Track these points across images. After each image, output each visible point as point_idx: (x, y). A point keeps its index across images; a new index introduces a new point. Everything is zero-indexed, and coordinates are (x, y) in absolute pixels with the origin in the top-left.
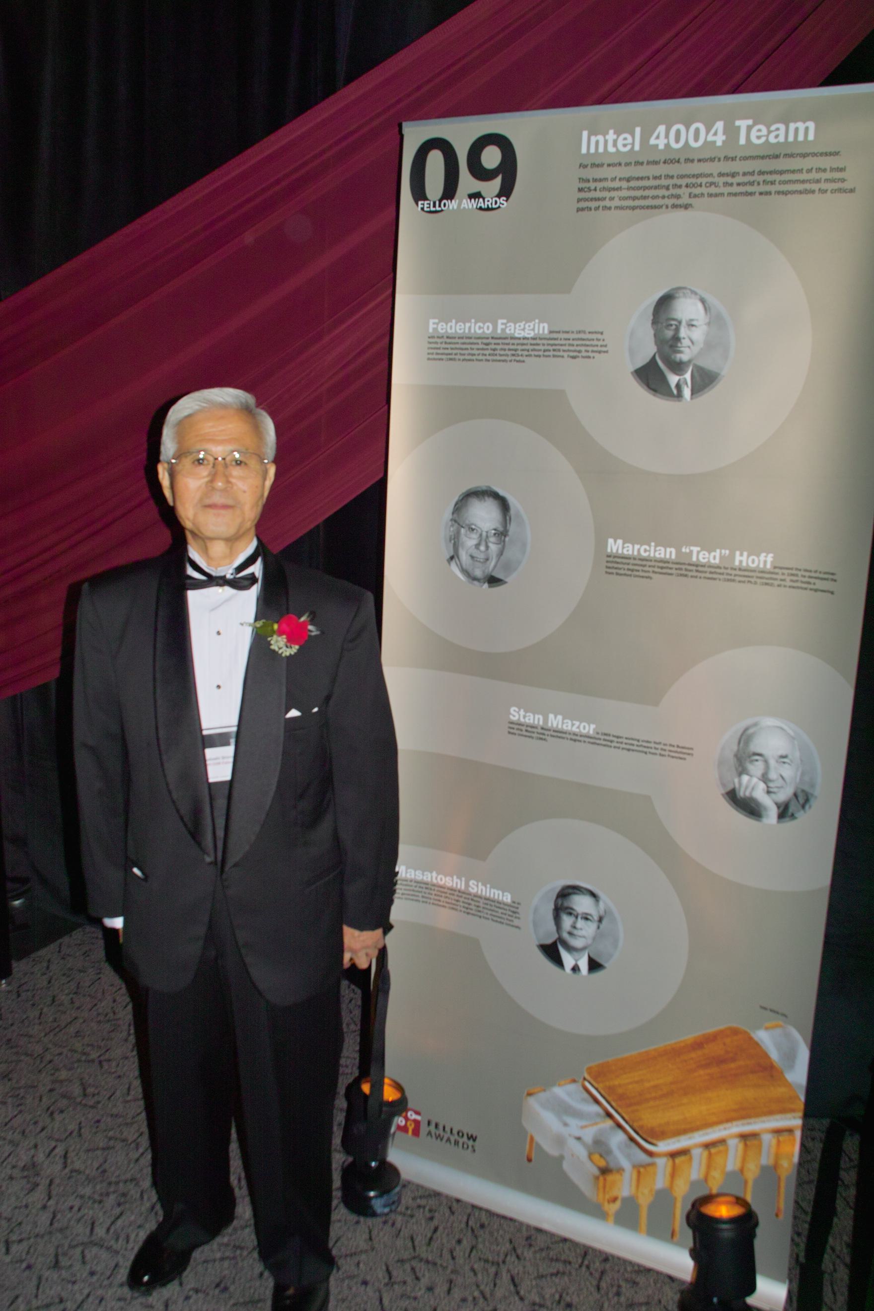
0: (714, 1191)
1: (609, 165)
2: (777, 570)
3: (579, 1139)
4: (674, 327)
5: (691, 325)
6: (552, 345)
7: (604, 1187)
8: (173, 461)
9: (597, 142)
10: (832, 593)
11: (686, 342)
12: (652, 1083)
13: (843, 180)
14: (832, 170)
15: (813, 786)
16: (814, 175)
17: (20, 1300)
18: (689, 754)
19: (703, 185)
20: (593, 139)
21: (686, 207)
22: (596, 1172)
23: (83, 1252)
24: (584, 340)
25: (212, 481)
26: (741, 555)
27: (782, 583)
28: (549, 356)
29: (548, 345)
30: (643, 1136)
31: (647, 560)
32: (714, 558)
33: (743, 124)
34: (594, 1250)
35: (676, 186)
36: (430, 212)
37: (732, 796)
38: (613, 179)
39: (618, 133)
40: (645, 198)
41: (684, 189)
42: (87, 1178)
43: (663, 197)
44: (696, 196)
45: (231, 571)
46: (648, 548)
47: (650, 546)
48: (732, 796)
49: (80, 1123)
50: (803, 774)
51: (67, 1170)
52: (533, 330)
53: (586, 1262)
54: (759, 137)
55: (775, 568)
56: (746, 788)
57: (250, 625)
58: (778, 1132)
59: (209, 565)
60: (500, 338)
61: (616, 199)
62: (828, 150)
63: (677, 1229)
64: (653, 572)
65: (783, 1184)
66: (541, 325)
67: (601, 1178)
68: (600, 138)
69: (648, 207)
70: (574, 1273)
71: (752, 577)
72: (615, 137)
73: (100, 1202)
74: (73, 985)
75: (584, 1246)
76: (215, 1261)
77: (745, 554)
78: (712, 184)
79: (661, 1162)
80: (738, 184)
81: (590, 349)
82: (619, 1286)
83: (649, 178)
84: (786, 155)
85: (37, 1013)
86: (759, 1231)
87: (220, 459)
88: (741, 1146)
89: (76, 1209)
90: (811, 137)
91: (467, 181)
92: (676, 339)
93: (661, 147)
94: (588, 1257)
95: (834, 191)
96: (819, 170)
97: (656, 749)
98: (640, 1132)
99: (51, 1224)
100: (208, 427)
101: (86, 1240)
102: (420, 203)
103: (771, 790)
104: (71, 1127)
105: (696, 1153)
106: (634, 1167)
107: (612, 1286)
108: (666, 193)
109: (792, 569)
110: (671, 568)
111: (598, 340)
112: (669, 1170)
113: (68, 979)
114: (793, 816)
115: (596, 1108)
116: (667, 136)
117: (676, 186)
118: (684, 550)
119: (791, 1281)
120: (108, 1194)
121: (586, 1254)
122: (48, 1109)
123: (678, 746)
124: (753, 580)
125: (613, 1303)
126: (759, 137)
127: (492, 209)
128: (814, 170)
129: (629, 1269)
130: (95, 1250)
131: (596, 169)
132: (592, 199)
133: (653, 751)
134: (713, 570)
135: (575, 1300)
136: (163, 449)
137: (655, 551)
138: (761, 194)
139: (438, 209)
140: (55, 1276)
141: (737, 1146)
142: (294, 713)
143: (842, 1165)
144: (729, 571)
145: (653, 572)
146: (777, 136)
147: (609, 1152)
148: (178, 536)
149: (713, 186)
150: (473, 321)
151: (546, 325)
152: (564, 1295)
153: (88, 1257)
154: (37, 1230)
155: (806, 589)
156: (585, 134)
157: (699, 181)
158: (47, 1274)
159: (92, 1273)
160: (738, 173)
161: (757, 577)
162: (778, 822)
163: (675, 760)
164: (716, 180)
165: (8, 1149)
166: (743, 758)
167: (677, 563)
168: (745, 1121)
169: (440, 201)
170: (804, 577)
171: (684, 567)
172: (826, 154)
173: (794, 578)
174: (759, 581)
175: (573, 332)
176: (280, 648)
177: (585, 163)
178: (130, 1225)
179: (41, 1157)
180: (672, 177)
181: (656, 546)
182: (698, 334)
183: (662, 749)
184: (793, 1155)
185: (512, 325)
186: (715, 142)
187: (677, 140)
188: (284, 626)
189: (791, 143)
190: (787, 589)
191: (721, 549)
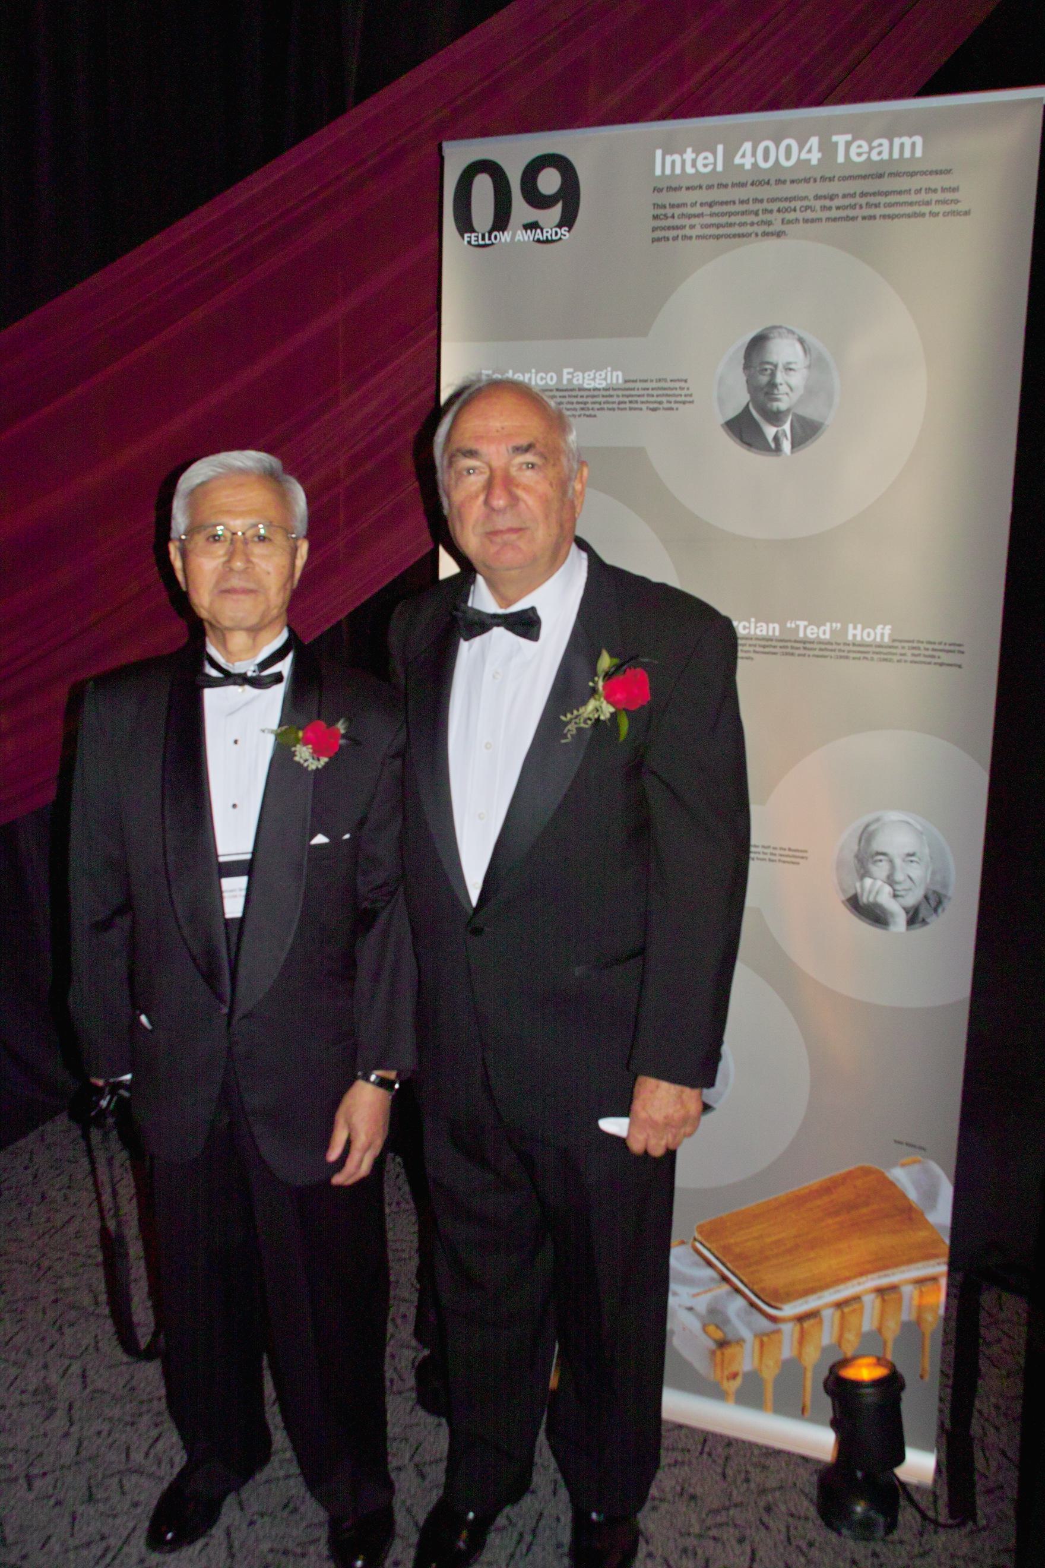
0: (849, 1353)
1: (688, 188)
2: (896, 644)
3: (690, 1309)
4: (769, 372)
5: (788, 369)
6: (628, 396)
7: (723, 1361)
8: (183, 537)
9: (673, 162)
10: (960, 666)
11: (783, 389)
12: (773, 1238)
13: (957, 202)
14: (943, 190)
15: (945, 885)
16: (923, 196)
17: (53, 1540)
18: (802, 858)
19: (798, 208)
20: (669, 159)
21: (779, 234)
22: (712, 1345)
23: (120, 1481)
24: (665, 389)
25: (229, 561)
26: (855, 628)
27: (903, 658)
28: (625, 409)
29: (623, 396)
30: (765, 1299)
31: (747, 639)
32: (824, 633)
33: (840, 139)
34: (715, 1435)
35: (765, 211)
36: (479, 246)
37: (855, 904)
38: (693, 205)
39: (697, 151)
40: (731, 225)
41: (775, 214)
42: (113, 1397)
43: (752, 224)
44: (790, 222)
45: (252, 668)
46: (747, 625)
47: (749, 622)
48: (855, 904)
49: (96, 1337)
50: (934, 873)
51: (88, 1390)
52: (605, 379)
53: (707, 1449)
54: (859, 155)
55: (894, 641)
56: (870, 892)
57: (272, 732)
58: (920, 1282)
59: (228, 661)
60: (566, 390)
61: (698, 227)
62: (939, 168)
63: (808, 1403)
64: (755, 652)
65: (928, 1343)
66: (615, 374)
67: (718, 1353)
68: (677, 157)
69: (734, 236)
70: (694, 1461)
71: (868, 652)
72: (694, 156)
73: (132, 1424)
74: (65, 1179)
75: (703, 1431)
76: (278, 1479)
77: (859, 626)
78: (807, 208)
79: (787, 1328)
80: (838, 208)
81: (672, 399)
82: (747, 1472)
83: (734, 203)
84: (891, 175)
85: (25, 1214)
86: (904, 1395)
87: (240, 534)
88: (878, 1302)
89: (104, 1434)
90: (919, 153)
91: (521, 210)
92: (772, 385)
93: (748, 167)
94: (709, 1443)
95: (946, 214)
96: (929, 190)
97: (765, 854)
98: (762, 1296)
99: (78, 1453)
100: (224, 497)
101: (122, 1467)
102: (466, 235)
103: (898, 893)
104: (85, 1342)
105: (827, 1313)
106: (756, 1336)
107: (739, 1472)
108: (755, 219)
109: (913, 641)
110: (775, 647)
111: (682, 389)
112: (796, 1335)
113: (58, 1172)
114: (924, 922)
115: (709, 1272)
116: (754, 154)
117: (765, 211)
118: (789, 625)
119: (939, 1452)
120: (140, 1415)
121: (705, 1441)
122: (55, 1323)
123: (790, 850)
124: (869, 656)
125: (742, 1490)
126: (859, 155)
127: (553, 241)
128: (923, 191)
129: (756, 1452)
130: (135, 1478)
131: (672, 193)
132: (669, 228)
133: (761, 856)
134: (823, 647)
135: (699, 1490)
136: (174, 525)
137: (756, 627)
138: (864, 218)
139: (487, 242)
140: (92, 1512)
141: (873, 1302)
142: (320, 839)
143: (982, 1322)
144: (842, 647)
145: (755, 652)
146: (880, 153)
147: (727, 1321)
148: (197, 630)
149: (809, 211)
150: (533, 371)
151: (620, 373)
152: (686, 1486)
153: (127, 1485)
154: (62, 1461)
155: (929, 663)
156: (659, 153)
157: (793, 204)
158: (81, 1509)
159: (136, 1505)
160: (837, 196)
161: (874, 653)
162: (907, 929)
163: (786, 865)
164: (812, 203)
165: (14, 1371)
166: (865, 859)
167: (781, 641)
168: (882, 1273)
169: (490, 233)
170: (927, 649)
171: (789, 644)
172: (937, 172)
173: (916, 652)
174: (876, 657)
175: (652, 381)
176: (306, 761)
177: (660, 186)
178: (172, 1448)
179: (54, 1378)
180: (761, 201)
181: (756, 623)
182: (797, 380)
183: (772, 854)
184: (938, 1307)
185: (580, 374)
186: (809, 160)
187: (766, 158)
188: (310, 734)
189: (918, 159)
190: (909, 664)
191: (831, 623)
